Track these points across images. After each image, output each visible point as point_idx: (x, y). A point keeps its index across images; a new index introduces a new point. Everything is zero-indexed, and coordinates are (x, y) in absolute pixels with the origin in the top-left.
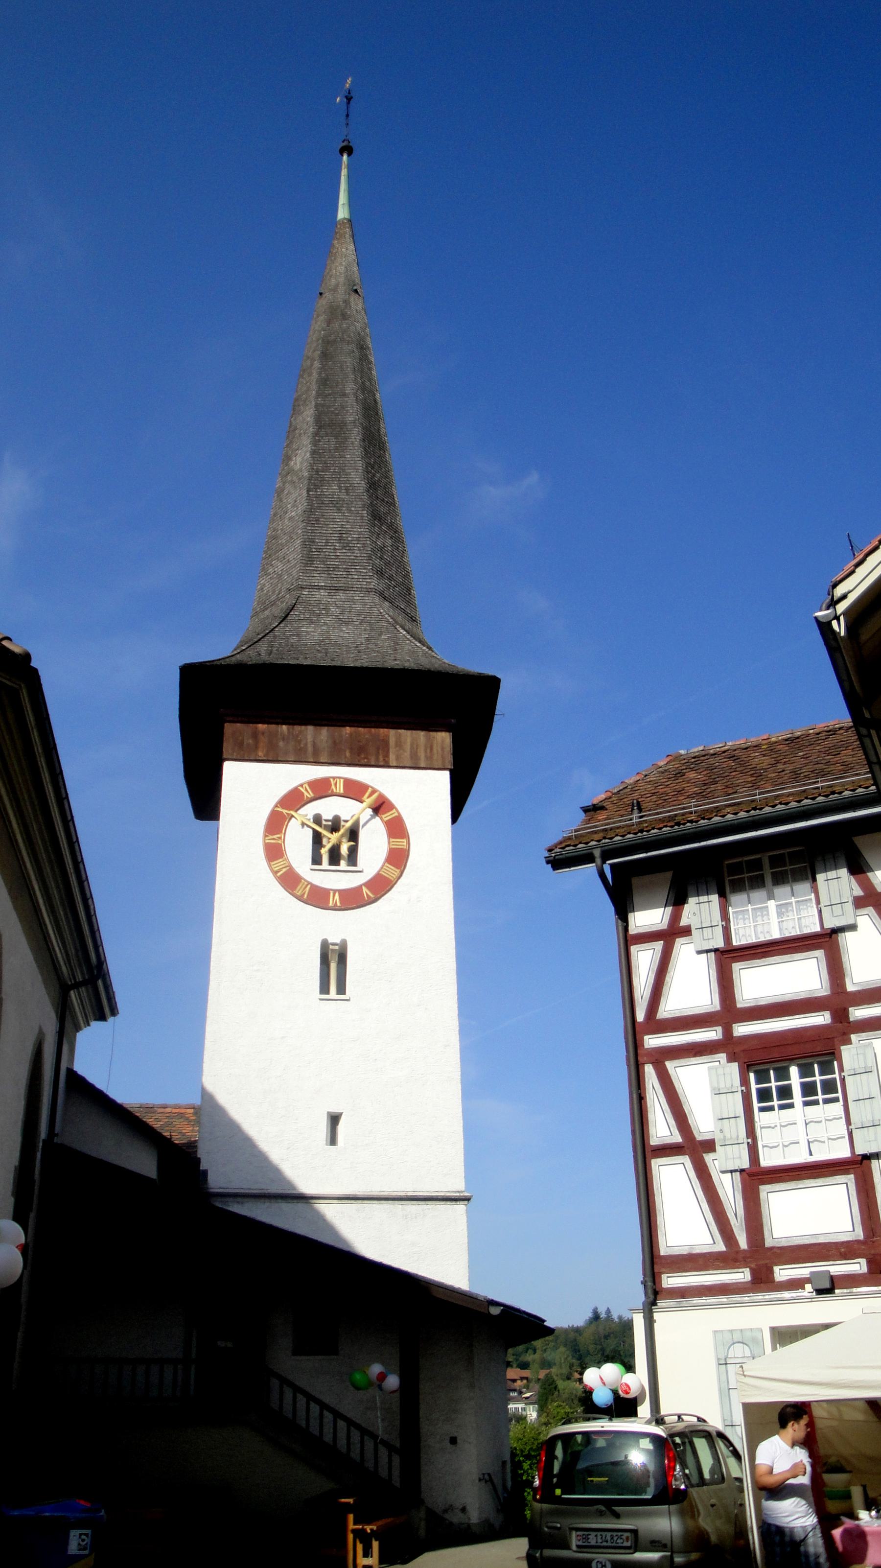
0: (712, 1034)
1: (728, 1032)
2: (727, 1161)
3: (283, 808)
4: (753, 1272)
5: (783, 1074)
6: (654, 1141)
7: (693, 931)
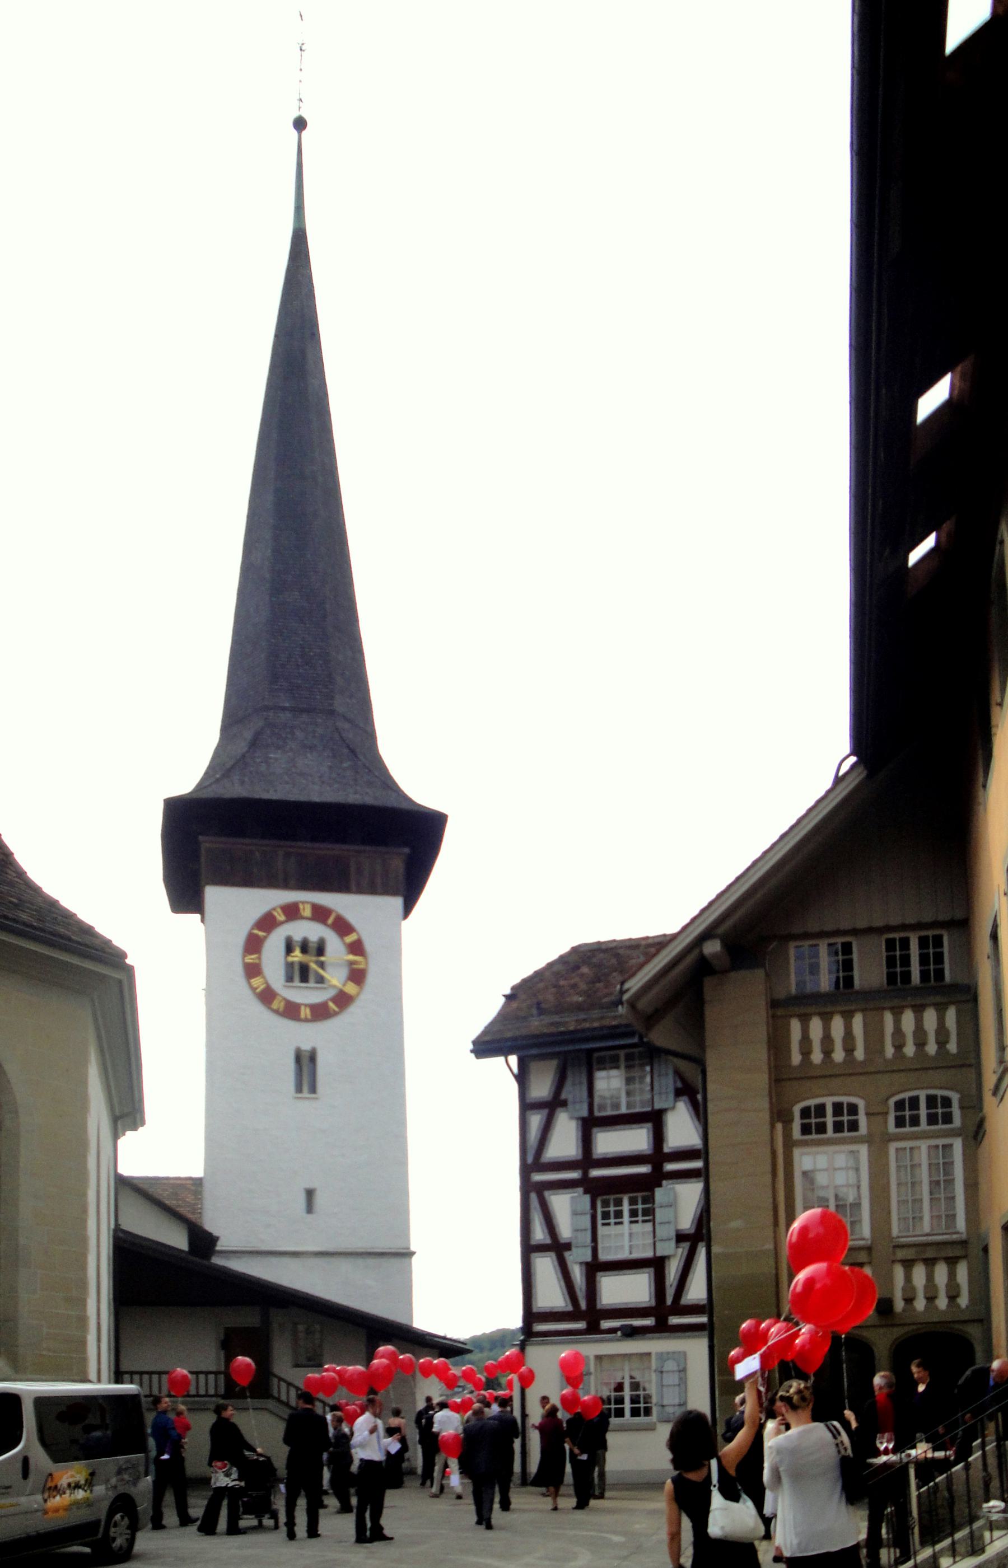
0: (574, 1175)
1: (585, 1174)
2: (577, 1259)
3: (260, 930)
4: (588, 1324)
5: (619, 1203)
6: (533, 1242)
7: (569, 1103)
